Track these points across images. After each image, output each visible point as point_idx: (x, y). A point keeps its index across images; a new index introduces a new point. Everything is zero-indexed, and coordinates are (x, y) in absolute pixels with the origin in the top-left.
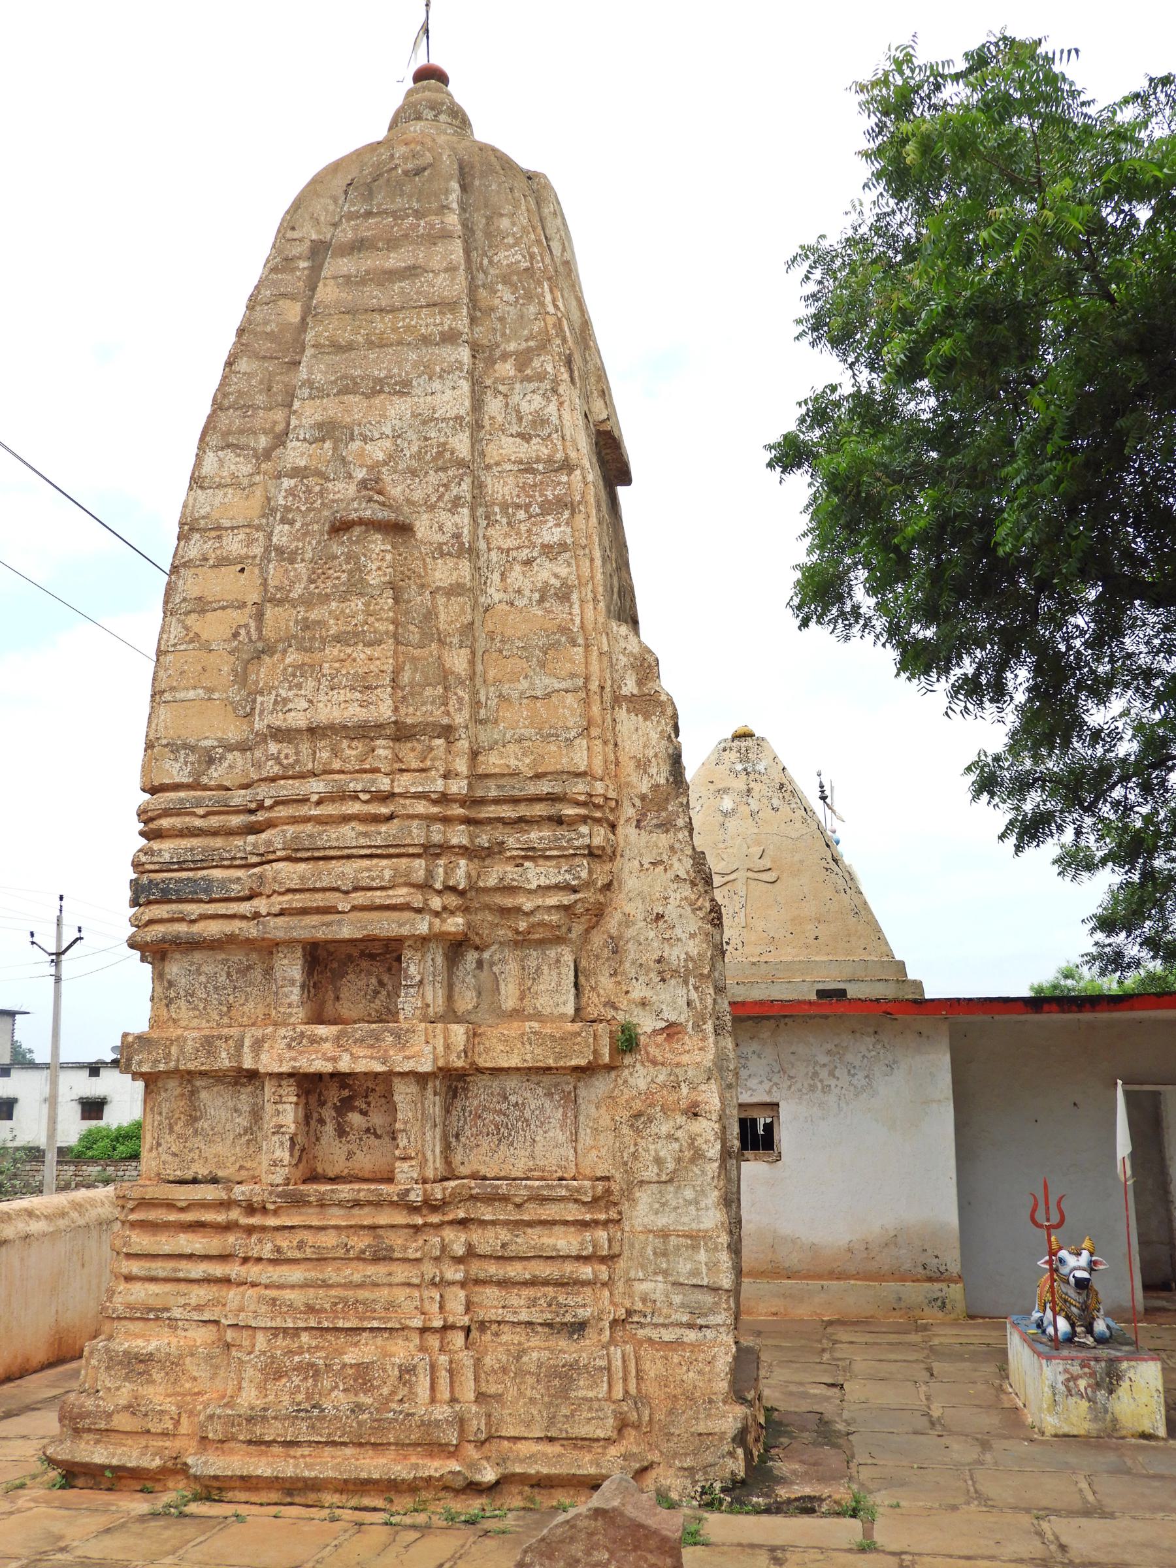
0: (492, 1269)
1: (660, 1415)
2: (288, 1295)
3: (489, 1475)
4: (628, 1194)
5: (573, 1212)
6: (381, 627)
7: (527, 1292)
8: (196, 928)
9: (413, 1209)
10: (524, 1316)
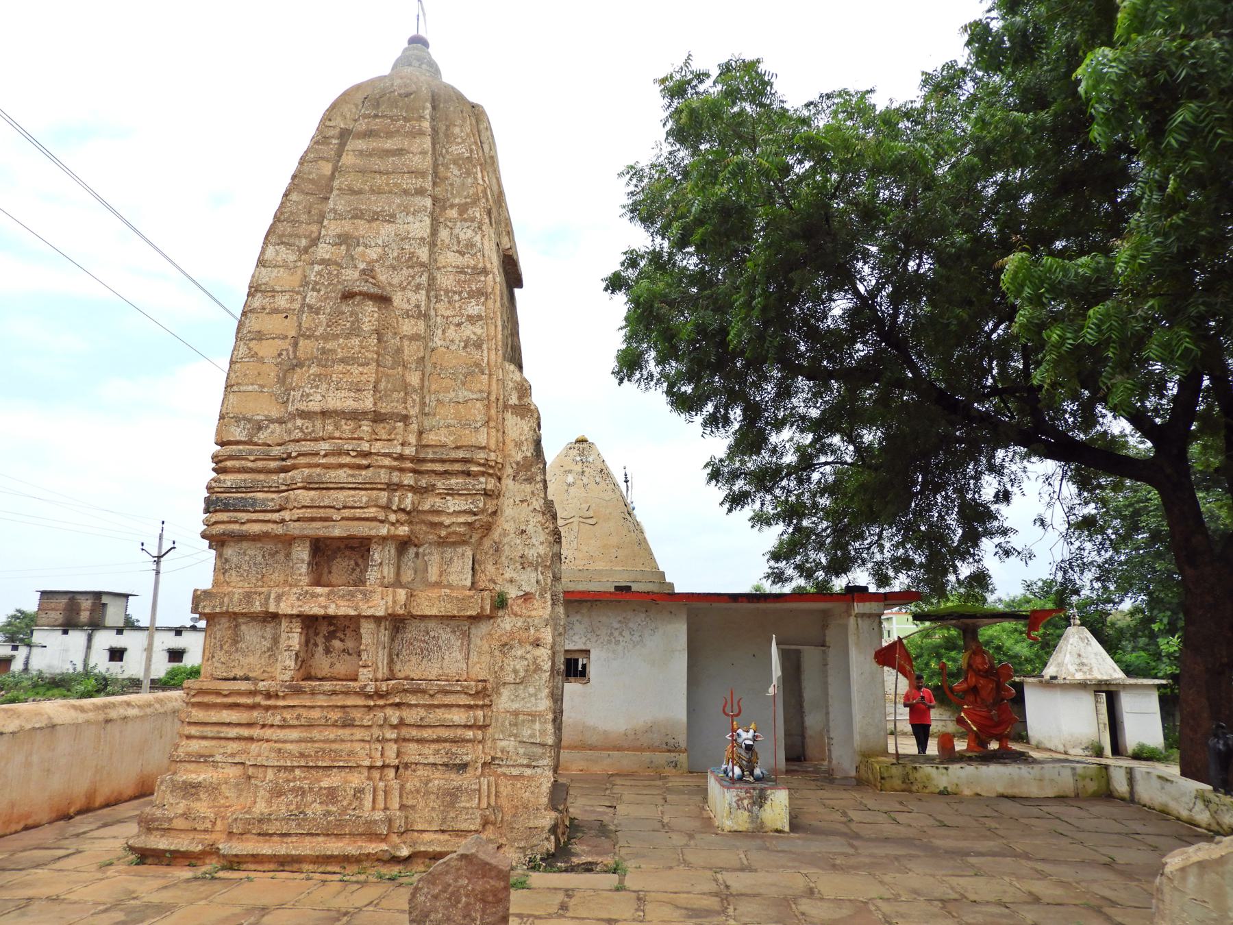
0: (414, 733)
2: (289, 746)
3: (405, 852)
4: (496, 690)
5: (464, 700)
7: (433, 746)
9: (368, 696)
10: (431, 760)
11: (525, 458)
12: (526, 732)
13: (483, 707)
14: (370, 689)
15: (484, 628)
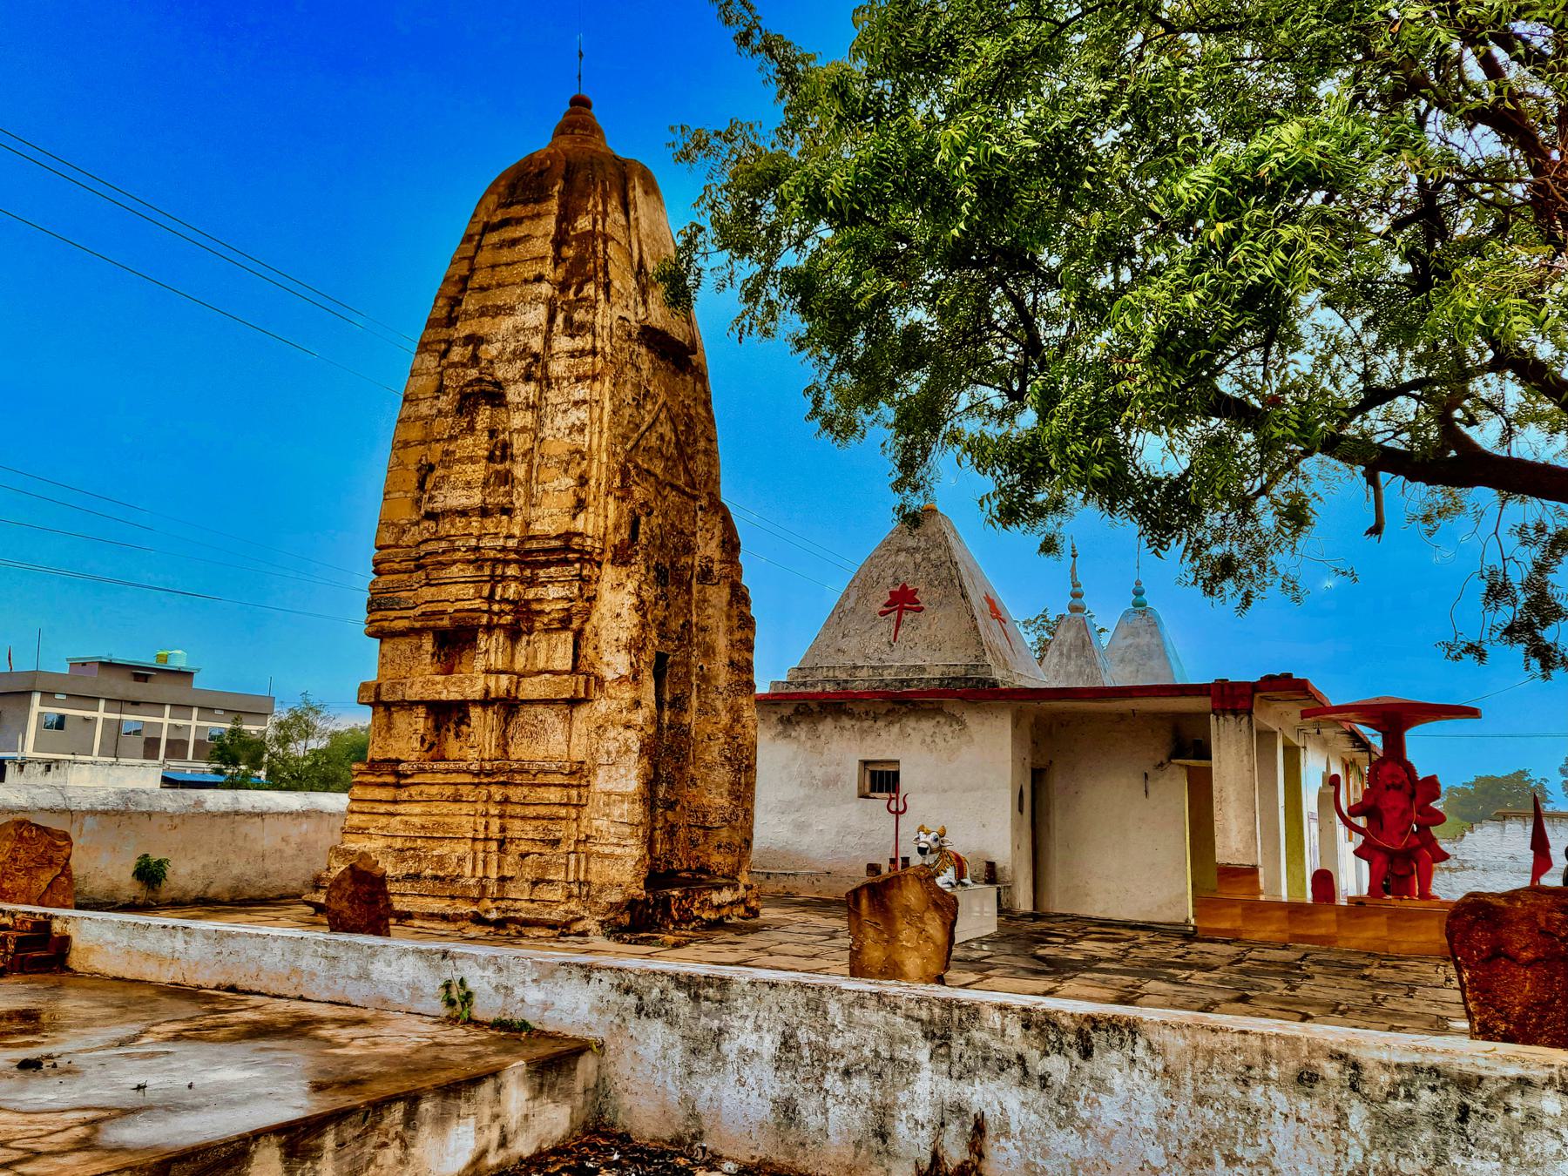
0: (518, 810)
1: (593, 893)
2: (414, 819)
3: (494, 915)
4: (592, 771)
5: (558, 779)
6: (481, 453)
7: (535, 823)
8: (393, 624)
9: (477, 775)
10: (530, 836)
11: (622, 541)
12: (616, 812)
13: (579, 786)
14: (475, 767)
15: (582, 712)
